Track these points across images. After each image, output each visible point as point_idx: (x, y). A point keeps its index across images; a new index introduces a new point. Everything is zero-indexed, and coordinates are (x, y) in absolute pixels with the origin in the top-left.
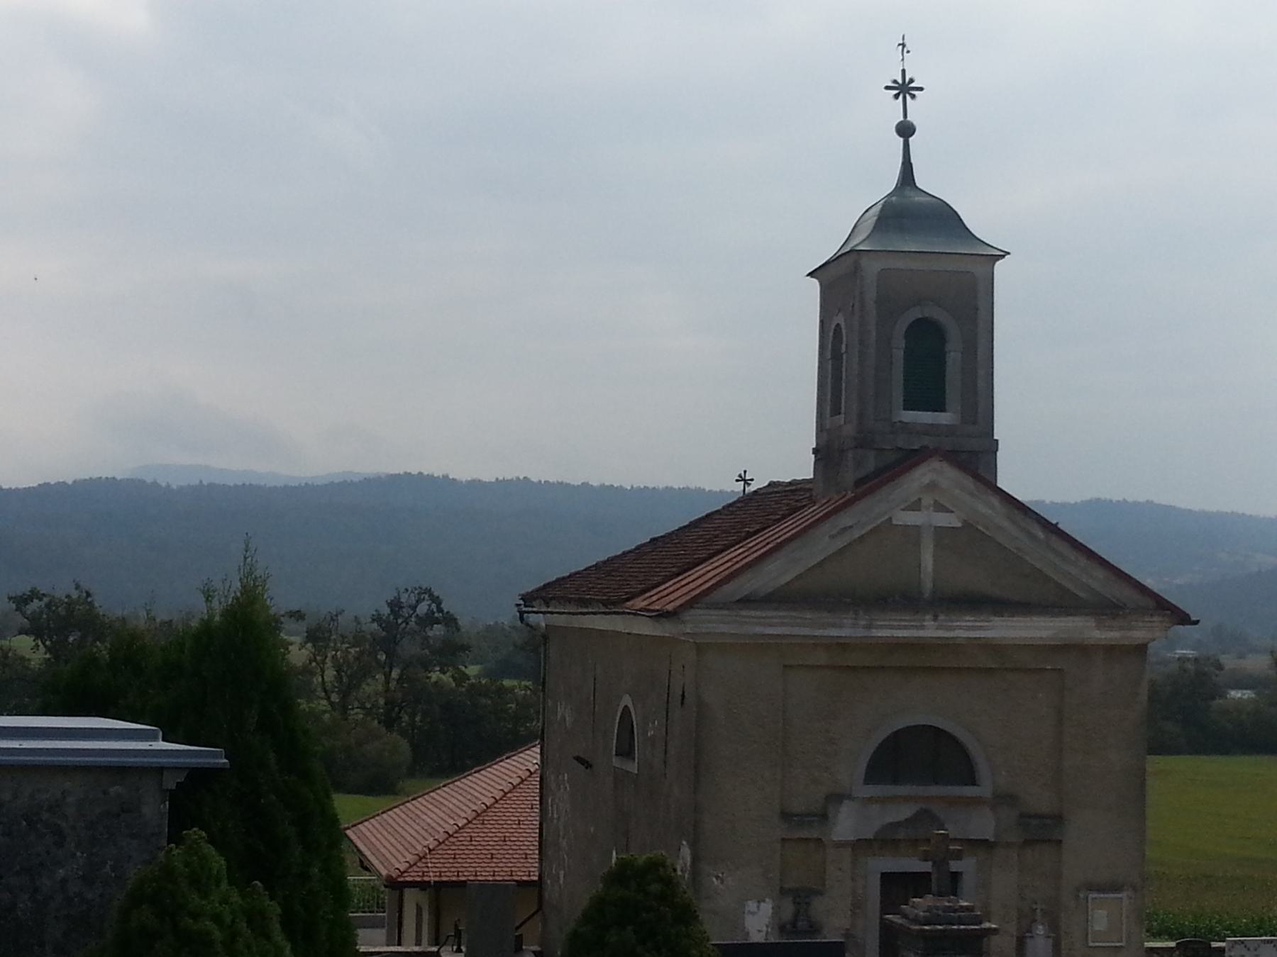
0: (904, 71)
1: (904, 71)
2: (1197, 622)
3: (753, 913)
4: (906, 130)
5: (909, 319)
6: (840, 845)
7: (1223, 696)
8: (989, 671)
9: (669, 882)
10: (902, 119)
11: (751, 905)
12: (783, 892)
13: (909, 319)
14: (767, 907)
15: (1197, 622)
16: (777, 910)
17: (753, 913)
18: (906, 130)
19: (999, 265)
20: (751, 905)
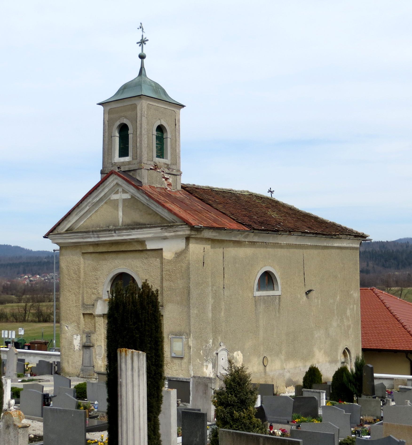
0: (142, 36)
1: (142, 36)
2: (141, 23)
3: (76, 339)
4: (142, 57)
5: (137, 123)
6: (99, 316)
7: (13, 339)
8: (307, 233)
9: (149, 287)
10: (141, 52)
11: (75, 336)
12: (84, 332)
13: (137, 123)
14: (79, 337)
15: (141, 23)
16: (81, 339)
17: (76, 339)
18: (142, 57)
19: (182, 110)
20: (75, 336)
